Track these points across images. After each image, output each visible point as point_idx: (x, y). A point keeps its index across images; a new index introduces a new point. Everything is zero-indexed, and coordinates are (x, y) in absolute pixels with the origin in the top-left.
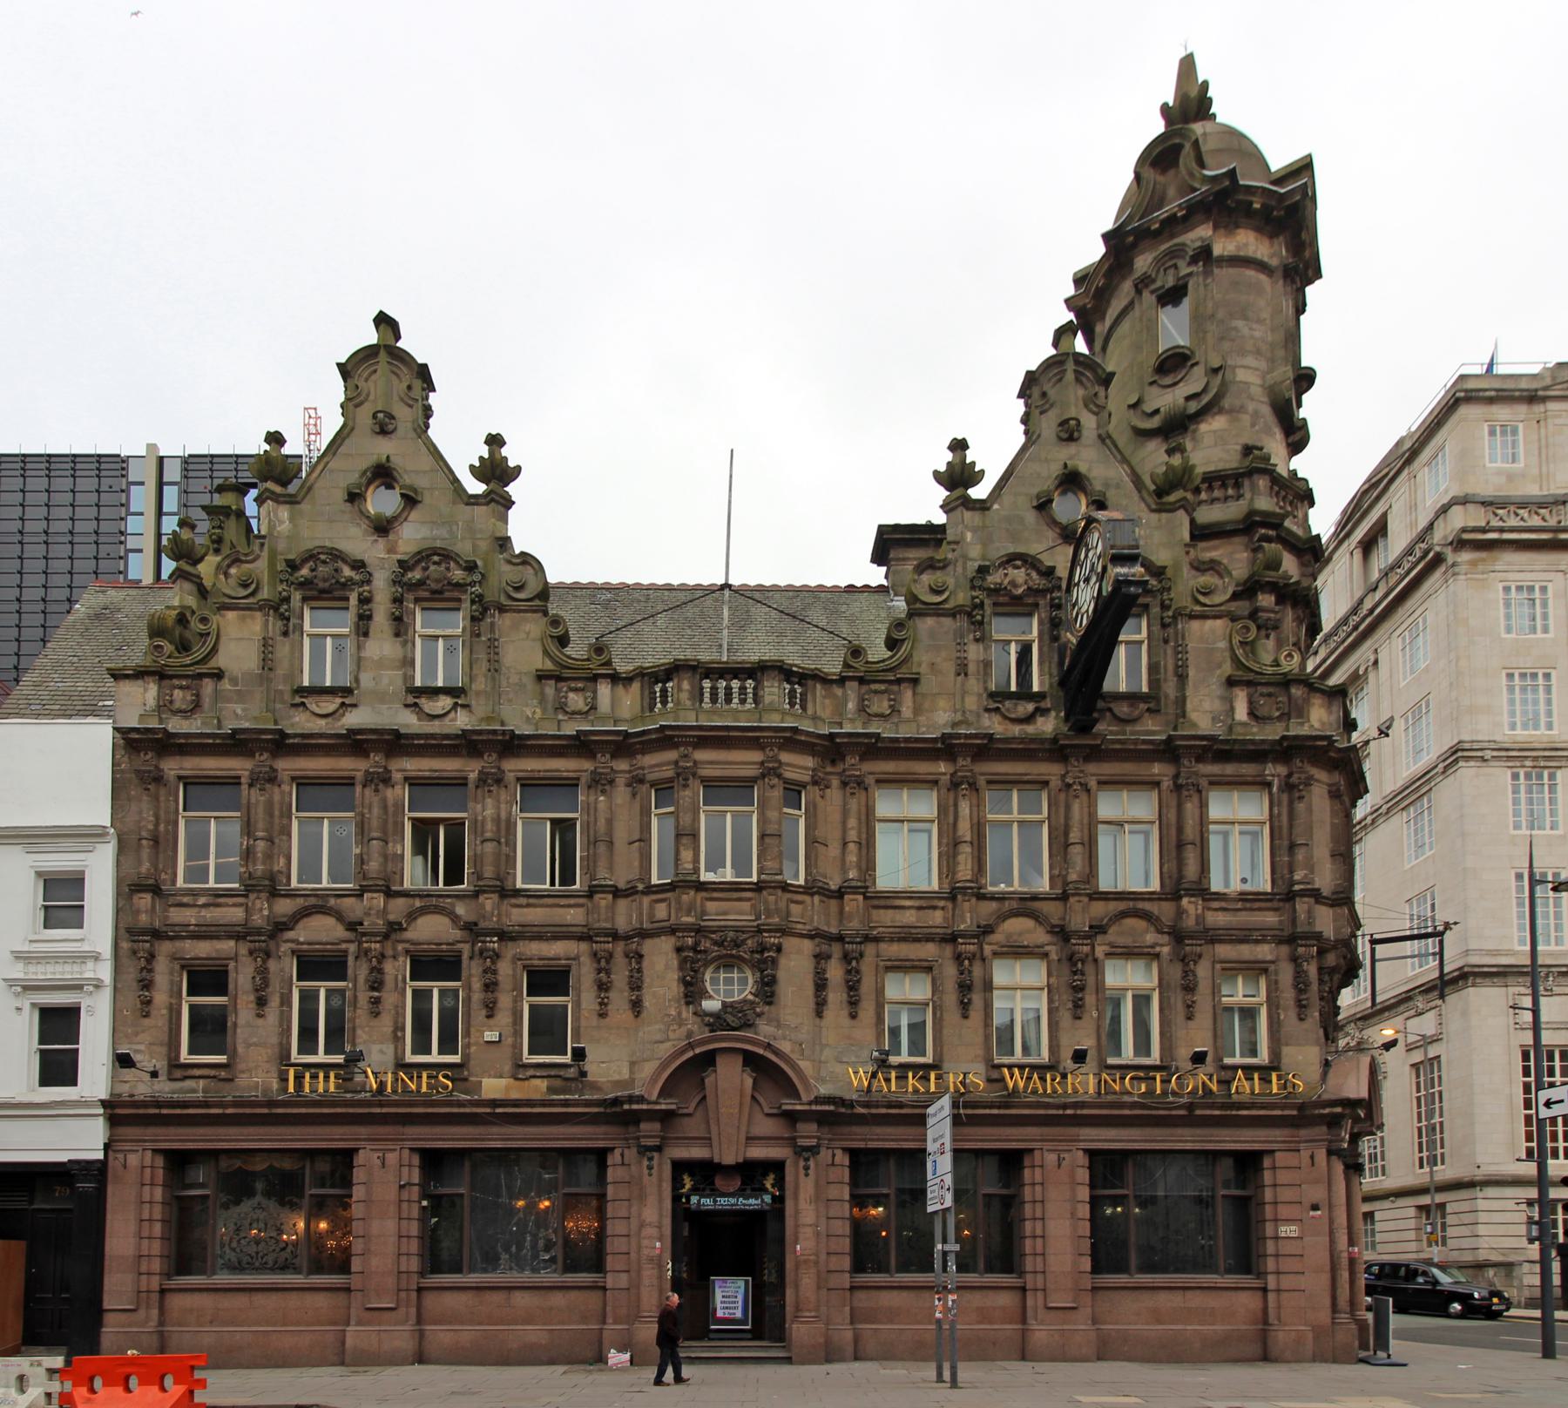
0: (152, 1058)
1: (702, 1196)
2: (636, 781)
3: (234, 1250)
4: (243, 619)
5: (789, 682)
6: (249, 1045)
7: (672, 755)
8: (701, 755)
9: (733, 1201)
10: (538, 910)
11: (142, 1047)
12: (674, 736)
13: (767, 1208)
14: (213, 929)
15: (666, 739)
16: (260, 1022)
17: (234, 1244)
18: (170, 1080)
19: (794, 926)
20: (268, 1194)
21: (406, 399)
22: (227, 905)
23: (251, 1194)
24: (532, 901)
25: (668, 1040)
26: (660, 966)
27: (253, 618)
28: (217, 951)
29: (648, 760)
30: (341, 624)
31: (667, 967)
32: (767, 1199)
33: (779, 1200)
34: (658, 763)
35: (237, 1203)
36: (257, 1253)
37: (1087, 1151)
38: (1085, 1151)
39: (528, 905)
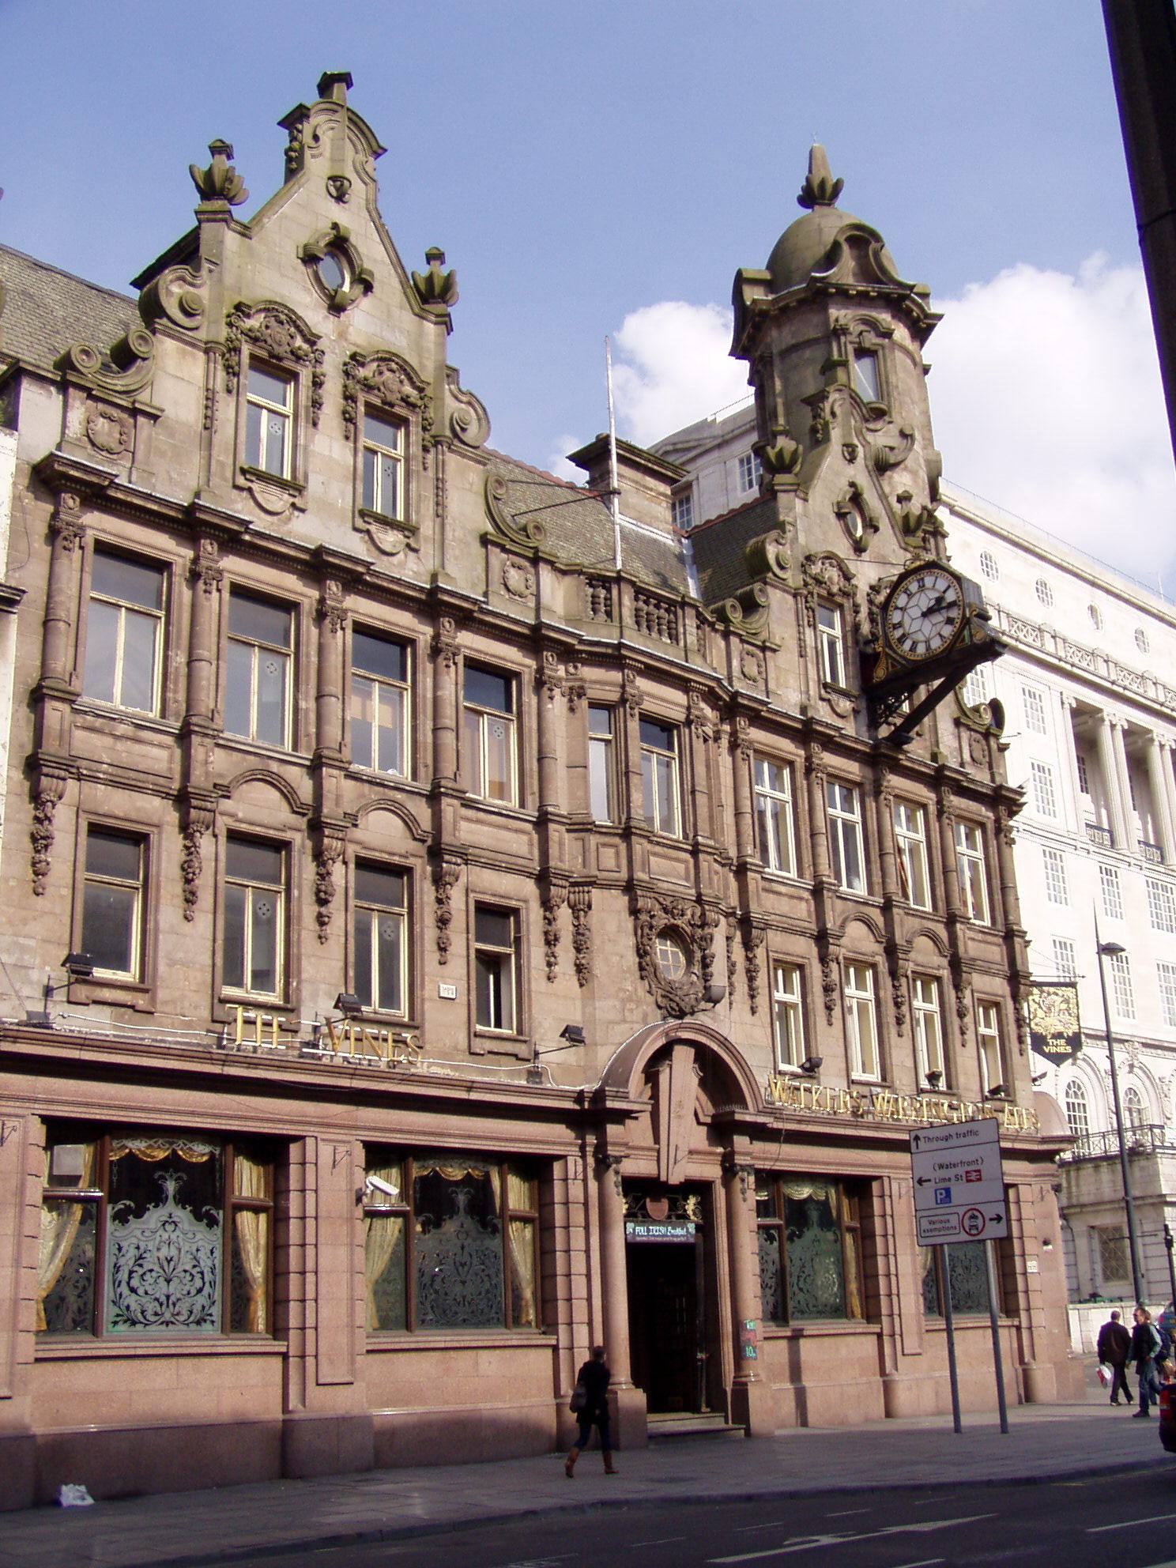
0: (45, 963)
1: (637, 1223)
2: (576, 693)
3: (133, 1290)
4: (184, 354)
5: (591, 585)
6: (172, 964)
7: (616, 676)
8: (643, 684)
9: (663, 1229)
10: (486, 828)
11: (32, 943)
12: (690, 680)
13: (692, 1240)
14: (132, 774)
15: (614, 658)
16: (187, 927)
17: (135, 1283)
18: (69, 1002)
19: (660, 884)
20: (182, 1199)
21: (359, 168)
22: (152, 744)
23: (159, 1198)
24: (481, 815)
25: (624, 1021)
26: (611, 926)
27: (194, 357)
28: (139, 810)
29: (589, 673)
30: (288, 399)
31: (619, 930)
32: (691, 1227)
33: (706, 1229)
34: (601, 680)
35: (139, 1213)
36: (168, 1297)
37: (46, 1120)
38: (362, 1141)
39: (478, 821)
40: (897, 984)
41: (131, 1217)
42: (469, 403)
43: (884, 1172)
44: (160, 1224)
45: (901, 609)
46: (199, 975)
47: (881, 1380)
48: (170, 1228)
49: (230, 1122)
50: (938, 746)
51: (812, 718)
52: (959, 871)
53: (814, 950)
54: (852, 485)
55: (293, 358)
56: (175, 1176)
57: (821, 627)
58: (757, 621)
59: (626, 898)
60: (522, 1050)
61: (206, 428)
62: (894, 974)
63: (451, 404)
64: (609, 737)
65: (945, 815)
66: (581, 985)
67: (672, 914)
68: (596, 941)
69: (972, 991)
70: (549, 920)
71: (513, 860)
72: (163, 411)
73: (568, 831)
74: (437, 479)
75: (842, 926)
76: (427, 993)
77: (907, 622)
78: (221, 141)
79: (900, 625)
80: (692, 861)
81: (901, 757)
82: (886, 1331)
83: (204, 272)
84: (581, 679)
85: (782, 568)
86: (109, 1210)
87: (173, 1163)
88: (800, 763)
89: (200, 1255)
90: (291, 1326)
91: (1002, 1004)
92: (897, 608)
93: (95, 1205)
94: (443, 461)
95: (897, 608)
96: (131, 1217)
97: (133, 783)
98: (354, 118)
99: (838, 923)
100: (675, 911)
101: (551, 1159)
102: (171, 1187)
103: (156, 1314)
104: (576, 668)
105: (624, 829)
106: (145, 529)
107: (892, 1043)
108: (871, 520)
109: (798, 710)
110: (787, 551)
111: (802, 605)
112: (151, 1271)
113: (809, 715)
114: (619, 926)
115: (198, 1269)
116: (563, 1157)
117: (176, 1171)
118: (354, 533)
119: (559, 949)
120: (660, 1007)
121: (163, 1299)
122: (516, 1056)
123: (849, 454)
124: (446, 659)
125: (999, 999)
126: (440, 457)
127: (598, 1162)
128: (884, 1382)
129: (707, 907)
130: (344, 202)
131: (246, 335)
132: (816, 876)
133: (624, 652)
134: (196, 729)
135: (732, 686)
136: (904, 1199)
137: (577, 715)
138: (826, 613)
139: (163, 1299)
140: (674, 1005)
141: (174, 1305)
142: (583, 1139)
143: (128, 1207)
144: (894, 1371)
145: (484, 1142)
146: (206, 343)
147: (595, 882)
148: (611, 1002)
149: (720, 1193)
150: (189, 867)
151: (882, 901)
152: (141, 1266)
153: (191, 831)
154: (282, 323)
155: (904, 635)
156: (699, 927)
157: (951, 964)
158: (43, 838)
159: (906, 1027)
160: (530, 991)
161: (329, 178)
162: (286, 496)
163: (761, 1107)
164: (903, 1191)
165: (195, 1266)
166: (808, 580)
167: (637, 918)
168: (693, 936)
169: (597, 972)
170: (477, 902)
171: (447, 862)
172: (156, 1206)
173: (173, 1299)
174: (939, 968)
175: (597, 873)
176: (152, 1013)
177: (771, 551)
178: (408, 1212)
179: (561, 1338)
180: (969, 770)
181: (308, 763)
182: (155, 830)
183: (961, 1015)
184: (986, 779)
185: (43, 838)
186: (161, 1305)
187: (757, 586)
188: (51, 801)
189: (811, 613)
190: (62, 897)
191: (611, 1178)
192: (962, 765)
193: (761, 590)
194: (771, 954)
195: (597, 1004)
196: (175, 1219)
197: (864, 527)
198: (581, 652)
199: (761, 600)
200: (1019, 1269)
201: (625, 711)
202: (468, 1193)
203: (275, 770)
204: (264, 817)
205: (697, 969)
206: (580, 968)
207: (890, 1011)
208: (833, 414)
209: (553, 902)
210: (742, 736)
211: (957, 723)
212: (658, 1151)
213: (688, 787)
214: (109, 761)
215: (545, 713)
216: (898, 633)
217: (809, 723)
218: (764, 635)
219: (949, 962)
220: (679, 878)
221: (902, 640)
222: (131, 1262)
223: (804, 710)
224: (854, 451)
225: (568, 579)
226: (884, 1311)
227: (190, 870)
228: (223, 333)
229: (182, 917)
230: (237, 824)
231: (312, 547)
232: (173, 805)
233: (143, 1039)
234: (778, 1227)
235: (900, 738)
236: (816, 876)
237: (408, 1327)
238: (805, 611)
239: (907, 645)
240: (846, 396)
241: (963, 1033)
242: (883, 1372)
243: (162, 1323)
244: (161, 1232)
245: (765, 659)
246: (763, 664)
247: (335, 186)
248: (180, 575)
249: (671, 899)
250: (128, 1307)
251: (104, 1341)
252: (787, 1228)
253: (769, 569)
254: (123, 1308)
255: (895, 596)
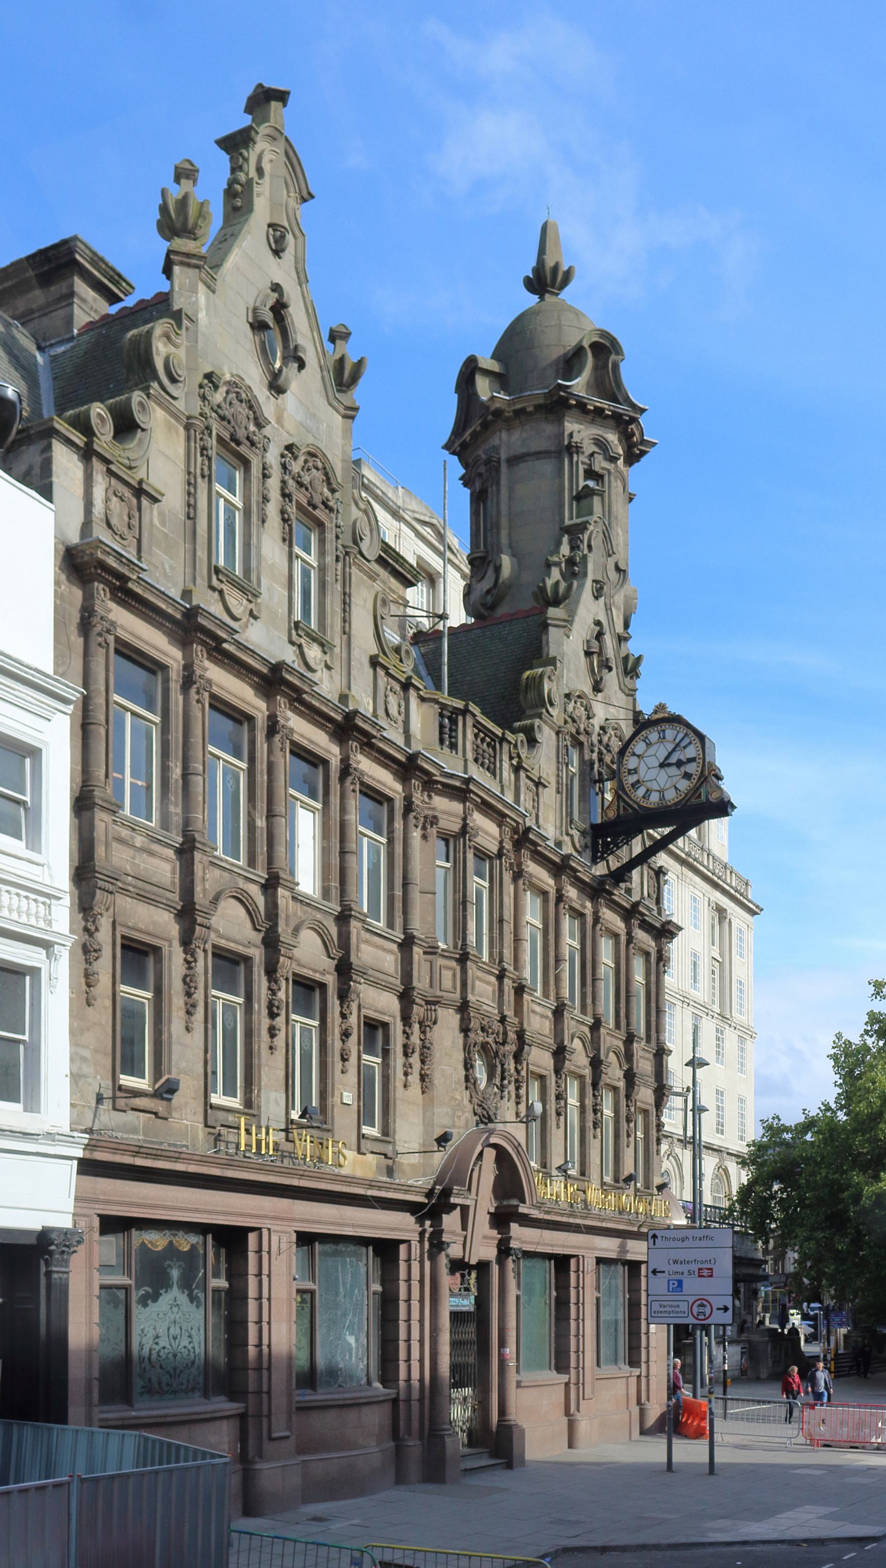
7: (457, 807)
12: (507, 816)
26: (448, 1043)
35: (155, 1297)
40: (275, 987)
41: (149, 1302)
42: (365, 512)
43: (579, 1252)
44: (169, 1307)
45: (638, 756)
46: (195, 1083)
47: (566, 1419)
48: (175, 1309)
49: (170, 1213)
50: (349, 688)
51: (198, 607)
52: (358, 853)
53: (174, 930)
54: (276, 288)
55: (248, 444)
56: (178, 1264)
57: (218, 487)
58: (131, 449)
59: (458, 1016)
60: (389, 1150)
61: (189, 518)
62: (595, 1085)
63: (355, 513)
64: (448, 865)
65: (413, 814)
66: (423, 1092)
67: (487, 1033)
68: (437, 1053)
69: (527, 1064)
70: (407, 1034)
71: (148, 887)
72: (163, 495)
73: (425, 953)
74: (345, 594)
75: (216, 900)
76: (337, 1099)
77: (642, 770)
78: (188, 161)
79: (635, 771)
80: (458, 968)
81: (615, 892)
82: (573, 1380)
83: (183, 332)
84: (434, 809)
85: (173, 380)
86: (135, 1296)
87: (171, 1251)
88: (335, 763)
89: (193, 1333)
90: (250, 1390)
91: (165, 951)
92: (634, 754)
93: (309, 1295)
94: (350, 574)
95: (634, 754)
96: (149, 1302)
97: (153, 897)
98: (291, 154)
99: (211, 896)
100: (490, 1031)
101: (396, 1243)
102: (175, 1274)
103: (168, 1385)
104: (430, 797)
105: (461, 955)
106: (150, 627)
107: (336, 1078)
108: (296, 348)
109: (179, 593)
110: (180, 355)
111: (195, 447)
112: (164, 1348)
113: (194, 603)
114: (453, 1042)
115: (192, 1345)
116: (407, 1242)
117: (178, 1261)
118: (289, 645)
119: (98, 966)
120: (475, 1114)
121: (172, 1371)
122: (156, 1114)
123: (276, 242)
124: (352, 783)
125: (386, 1019)
126: (348, 569)
127: (431, 1245)
128: (569, 1420)
129: (508, 1028)
130: (280, 258)
131: (216, 412)
132: (558, 998)
133: (472, 787)
134: (419, 942)
135: (410, 748)
136: (284, 1256)
137: (429, 843)
138: (226, 468)
139: (172, 1371)
140: (485, 1113)
141: (179, 1376)
142: (422, 1225)
143: (147, 1293)
144: (576, 1413)
145: (186, 1214)
146: (188, 418)
147: (438, 1002)
148: (445, 1109)
149: (495, 1269)
150: (191, 981)
151: (592, 1021)
152: (157, 1344)
153: (193, 946)
154: (241, 401)
155: (638, 781)
156: (501, 1044)
157: (338, 969)
158: (95, 951)
159: (280, 1040)
160: (395, 1099)
161: (270, 226)
162: (245, 602)
163: (535, 1202)
164: (284, 1246)
165: (190, 1343)
166: (207, 410)
167: (466, 1036)
168: (497, 1052)
169: (436, 1082)
170: (123, 937)
171: (354, 981)
172: (166, 1292)
173: (178, 1371)
174: (250, 944)
175: (439, 993)
176: (166, 1119)
177: (160, 350)
178: (130, 1286)
179: (250, 1405)
180: (383, 722)
181: (400, 941)
182: (166, 944)
183: (628, 1120)
184: (400, 741)
185: (95, 951)
186: (171, 1377)
187: (137, 397)
188: (429, 1026)
189: (207, 463)
190: (106, 1008)
191: (443, 1261)
192: (375, 715)
193: (141, 404)
194: (530, 1066)
195: (436, 1110)
196: (178, 1302)
197: (285, 359)
198: (438, 782)
199: (139, 417)
200: (643, 1329)
201: (501, 864)
202: (180, 1266)
203: (241, 887)
204: (235, 933)
205: (497, 1081)
206: (423, 1078)
207: (590, 1116)
208: (260, 171)
209: (96, 910)
210: (198, 672)
211: (374, 663)
212: (465, 1238)
213: (496, 916)
214: (133, 874)
215: (410, 841)
216: (632, 779)
217: (192, 613)
218: (141, 474)
219: (263, 938)
220: (488, 999)
221: (636, 785)
222: (151, 1342)
223: (187, 594)
224: (283, 237)
225: (426, 705)
226: (573, 1364)
227: (192, 984)
228: (197, 406)
229: (184, 1029)
230: (219, 940)
231: (273, 662)
232: (175, 918)
233: (161, 1143)
234: (126, 1289)
235: (620, 875)
236: (558, 998)
237: (206, 1395)
238: (199, 459)
239: (641, 792)
240: (281, 151)
241: (344, 1059)
242: (567, 1413)
243: (172, 1393)
244: (170, 1314)
245: (139, 509)
246: (137, 514)
247: (274, 236)
248: (176, 681)
249: (488, 1019)
250: (150, 1380)
251: (136, 1410)
252: (138, 1288)
253: (156, 378)
254: (146, 1380)
255: (634, 742)
